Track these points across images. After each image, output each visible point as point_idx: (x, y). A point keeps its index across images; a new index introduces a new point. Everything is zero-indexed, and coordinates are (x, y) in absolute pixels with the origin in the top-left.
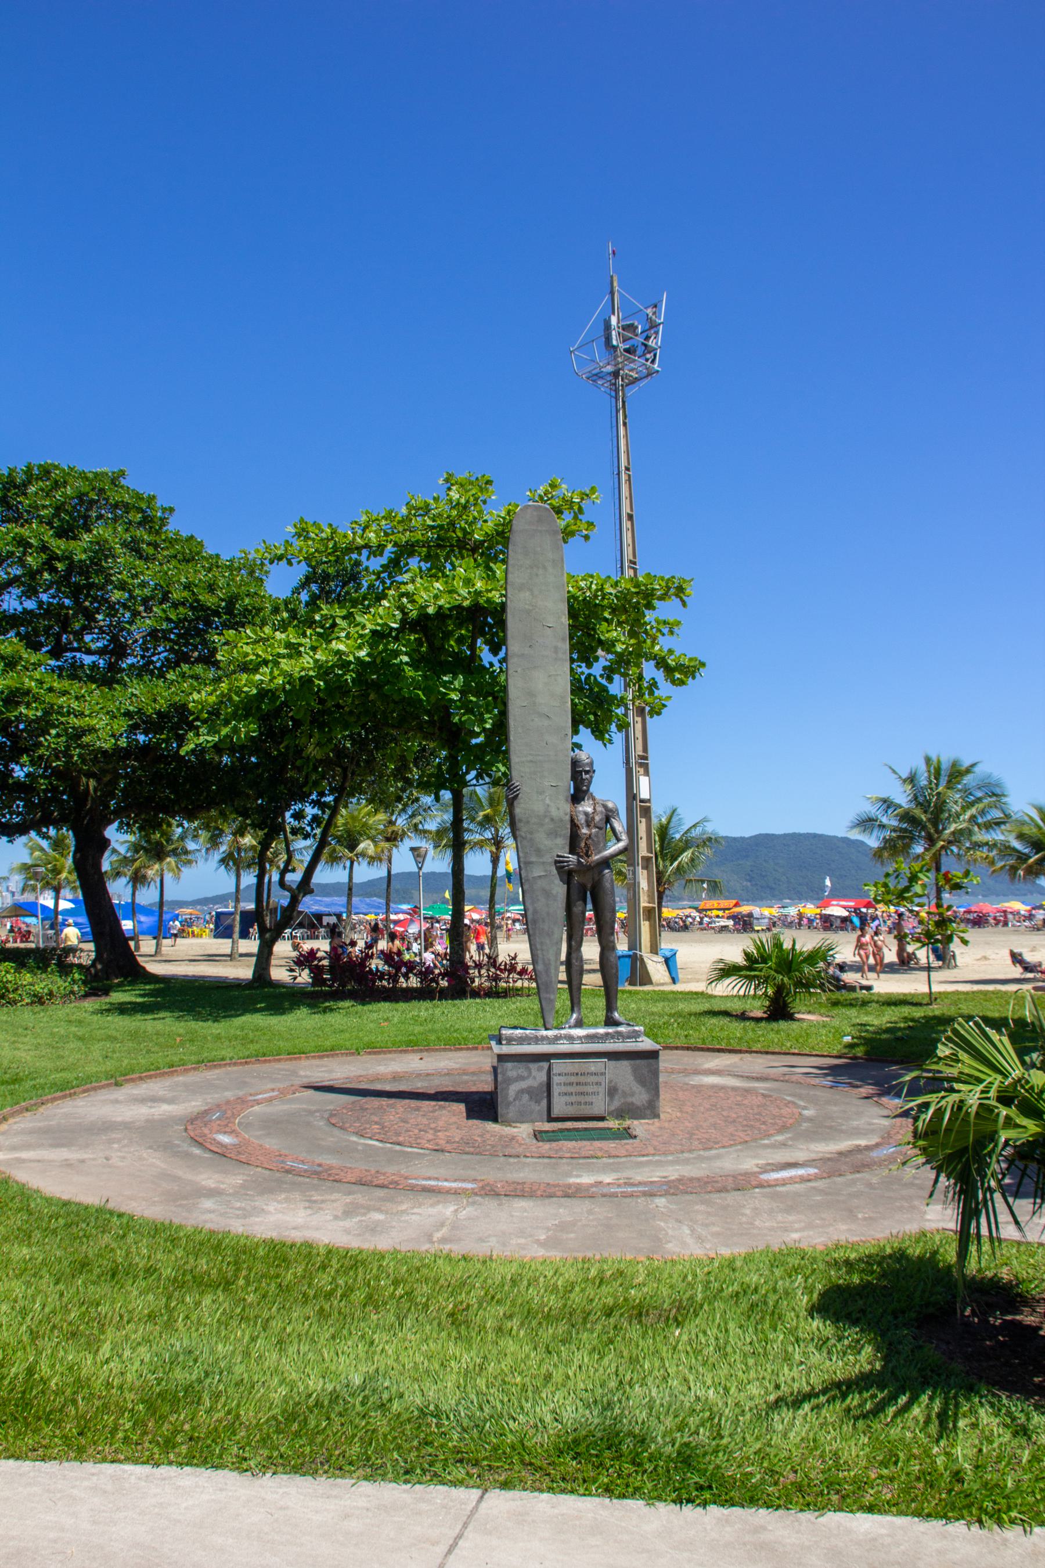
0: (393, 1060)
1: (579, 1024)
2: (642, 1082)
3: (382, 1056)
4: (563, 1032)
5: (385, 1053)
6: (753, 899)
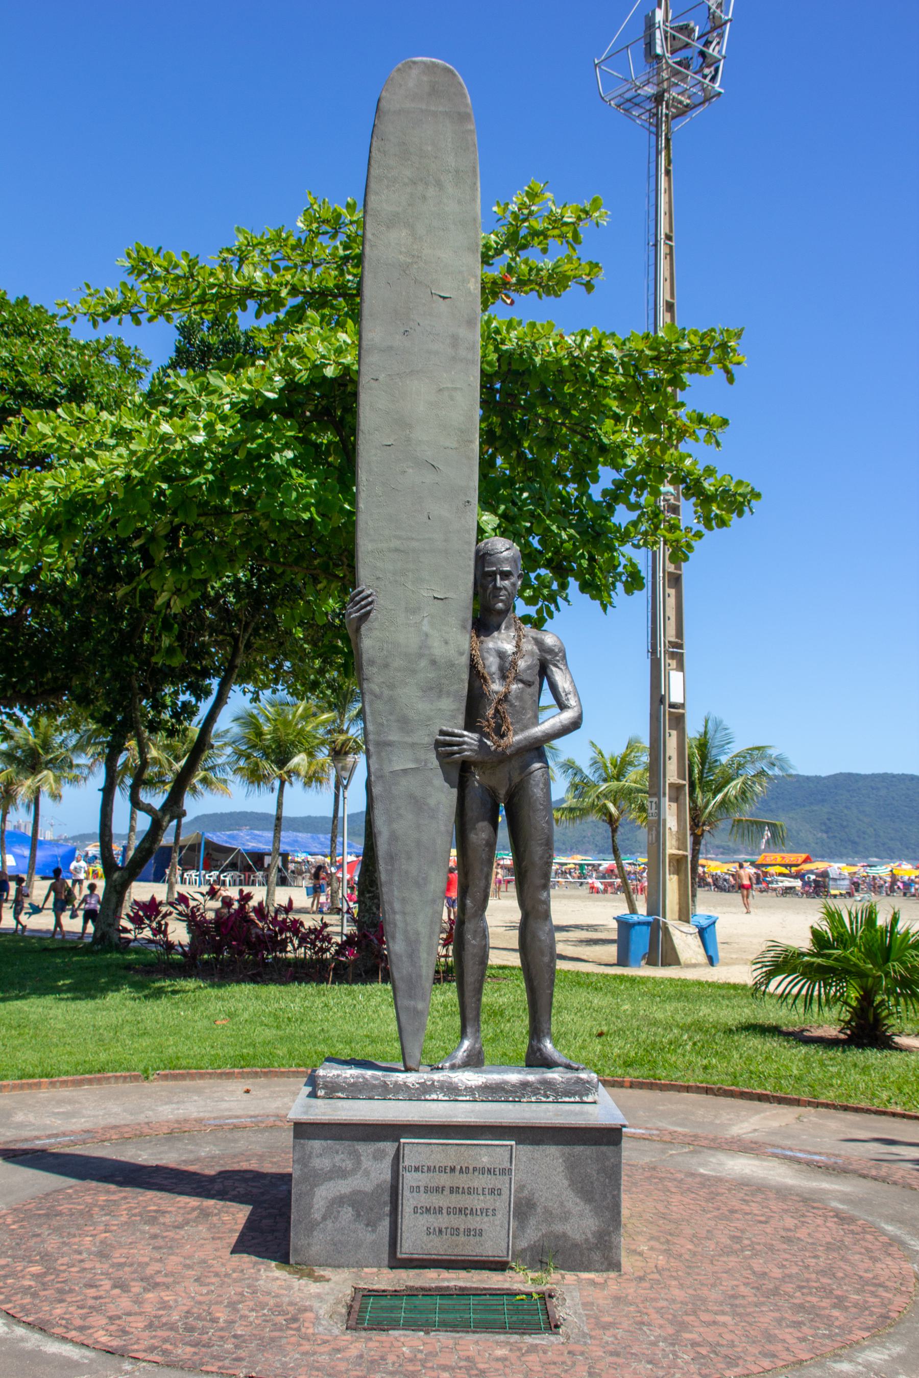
0: (199, 1091)
1: (474, 1061)
2: (585, 1192)
3: (187, 1083)
4: (437, 1076)
5: (192, 1077)
6: (832, 855)
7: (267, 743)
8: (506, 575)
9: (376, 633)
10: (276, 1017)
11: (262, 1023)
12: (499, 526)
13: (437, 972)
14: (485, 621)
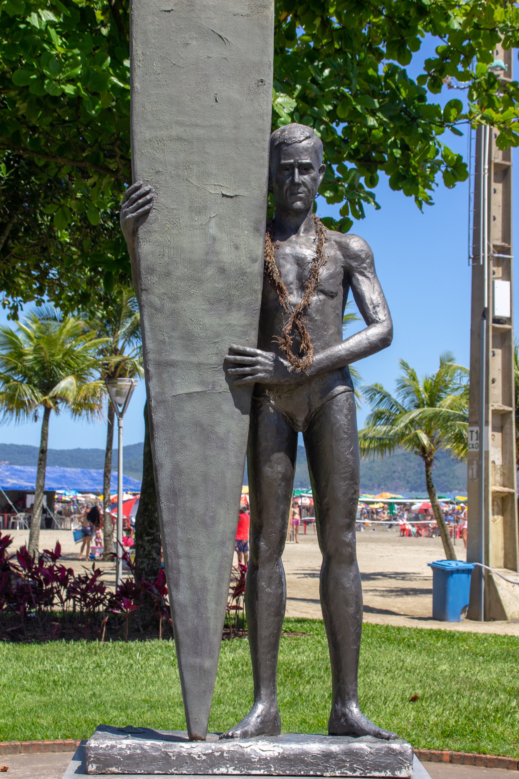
1: (269, 728)
4: (226, 746)
7: (28, 364)
8: (305, 169)
9: (156, 237)
10: (40, 681)
11: (23, 688)
12: (296, 109)
13: (226, 626)
14: (281, 222)
